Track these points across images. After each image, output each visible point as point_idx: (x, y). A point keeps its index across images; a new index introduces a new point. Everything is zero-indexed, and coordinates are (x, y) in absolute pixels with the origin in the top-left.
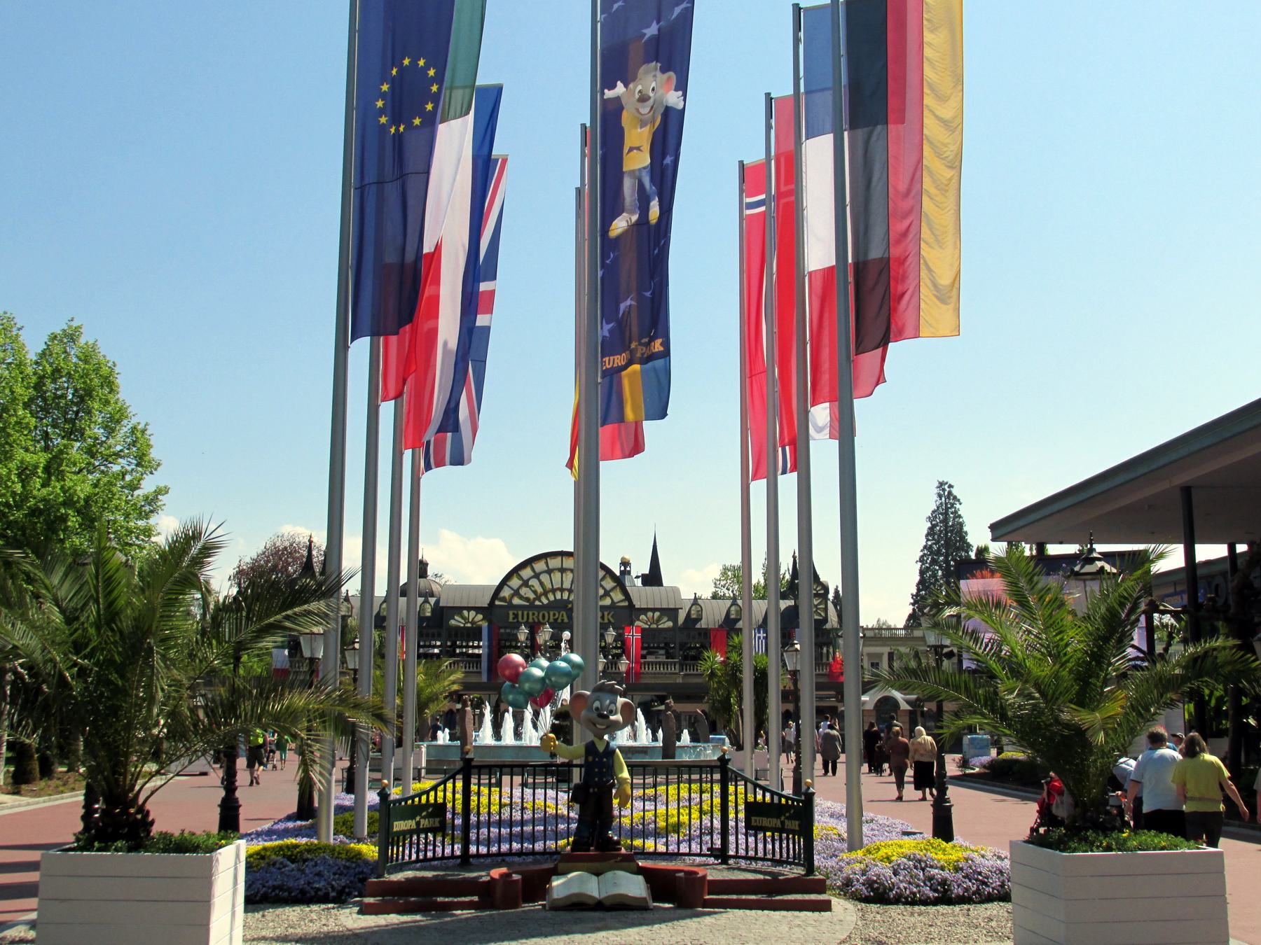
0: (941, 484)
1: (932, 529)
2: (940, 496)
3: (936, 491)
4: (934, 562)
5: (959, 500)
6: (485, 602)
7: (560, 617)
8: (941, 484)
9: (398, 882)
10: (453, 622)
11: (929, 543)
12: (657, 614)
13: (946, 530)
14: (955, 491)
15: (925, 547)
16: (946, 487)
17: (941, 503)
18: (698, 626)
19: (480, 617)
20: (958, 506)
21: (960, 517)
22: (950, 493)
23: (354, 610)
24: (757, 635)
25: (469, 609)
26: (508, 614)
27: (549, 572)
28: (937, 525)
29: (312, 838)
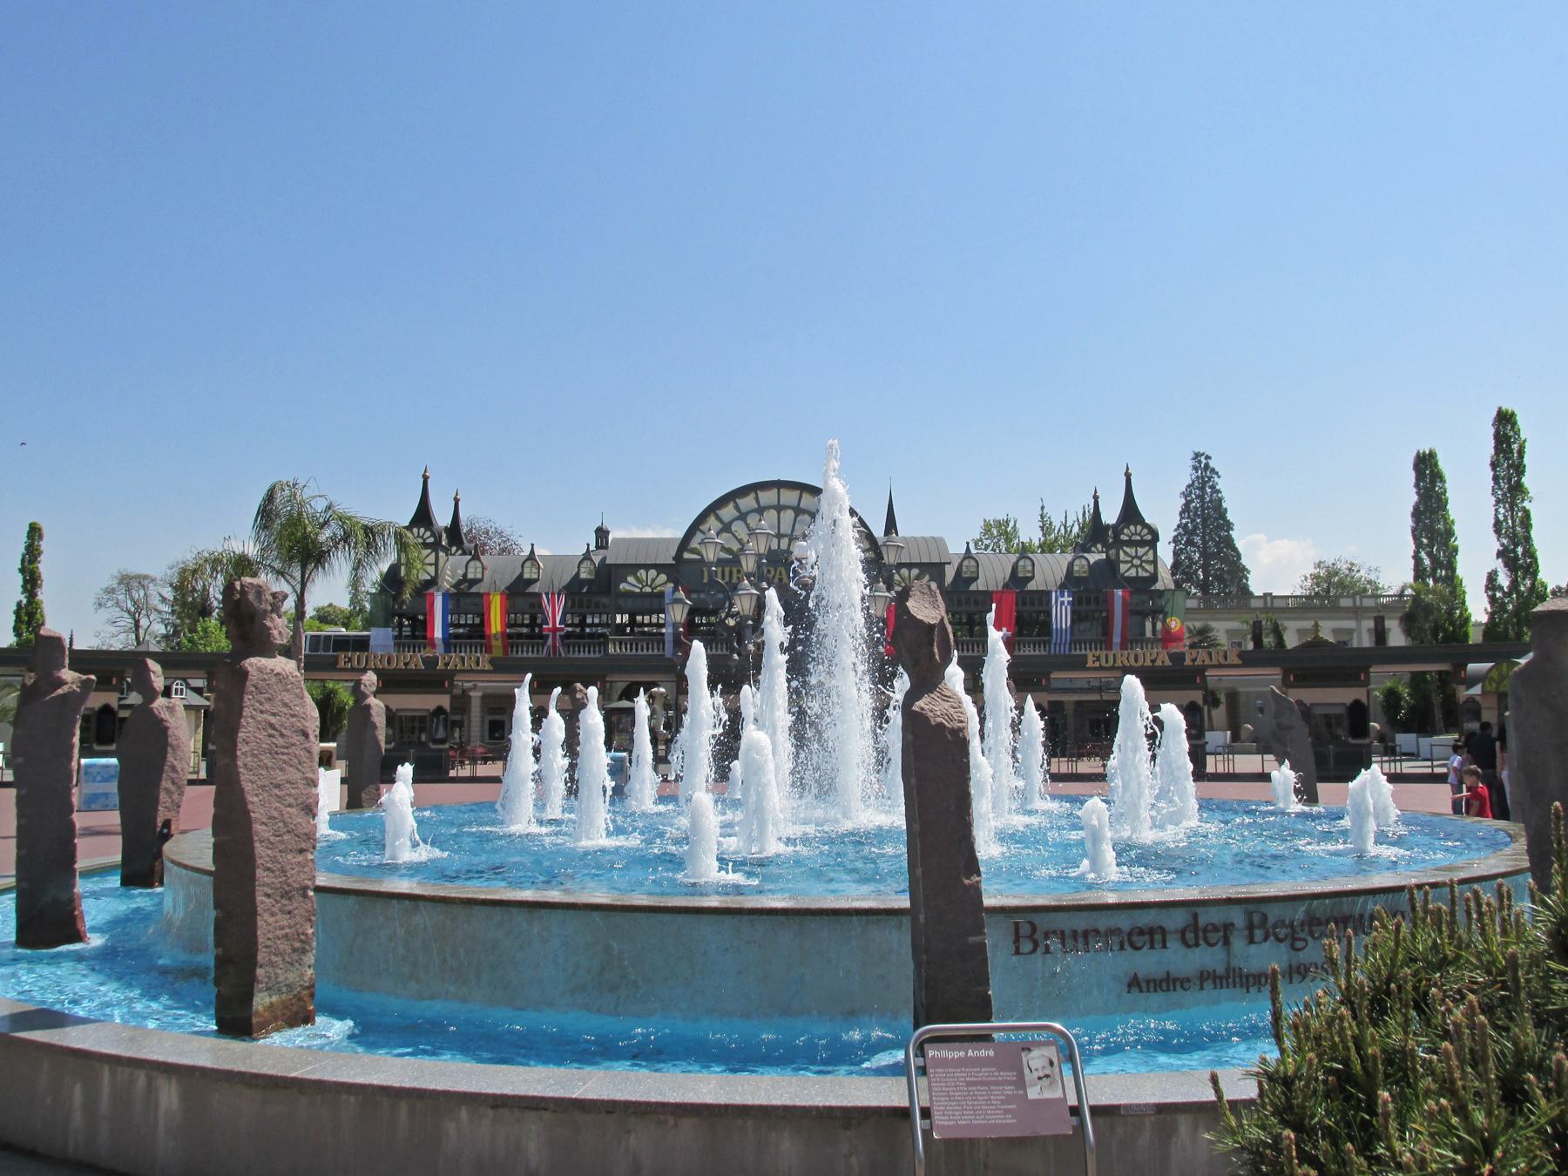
0: (1197, 455)
1: (1187, 505)
2: (1195, 469)
3: (1191, 463)
4: (1190, 542)
5: (1217, 473)
6: (668, 558)
7: (777, 576)
8: (1197, 455)
9: (74, 727)
10: (623, 586)
11: (1184, 521)
12: (915, 572)
13: (1202, 506)
14: (1212, 464)
15: (1179, 526)
16: (1203, 459)
17: (1197, 477)
18: (973, 587)
19: (663, 577)
20: (1216, 479)
21: (1219, 491)
22: (1207, 465)
23: (486, 572)
24: (1060, 599)
25: (647, 567)
26: (703, 571)
27: (760, 510)
28: (1192, 501)
29: (1393, 1102)
